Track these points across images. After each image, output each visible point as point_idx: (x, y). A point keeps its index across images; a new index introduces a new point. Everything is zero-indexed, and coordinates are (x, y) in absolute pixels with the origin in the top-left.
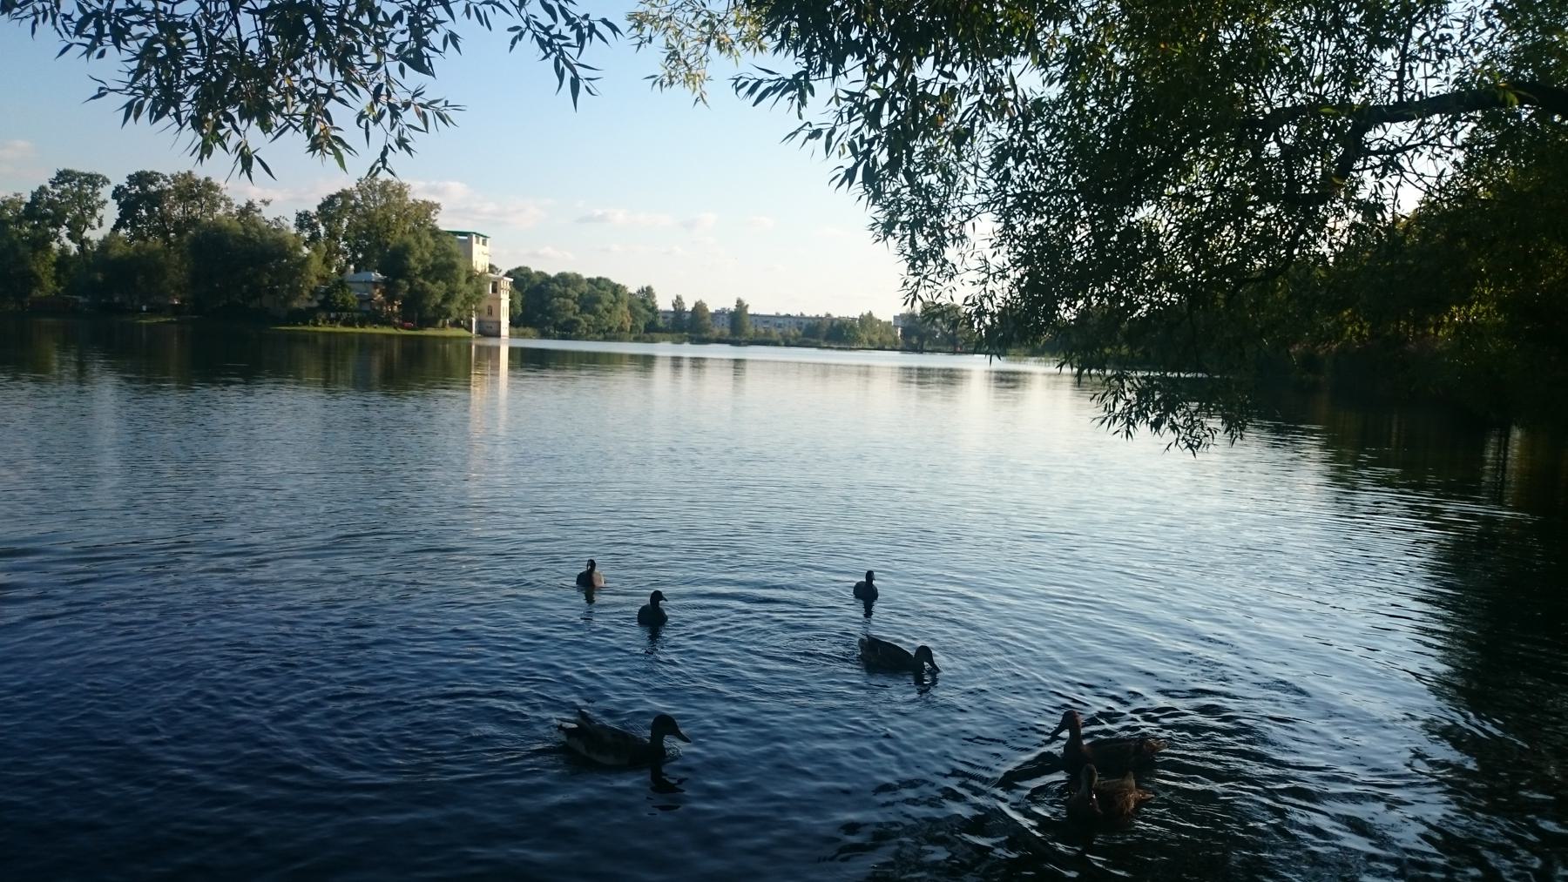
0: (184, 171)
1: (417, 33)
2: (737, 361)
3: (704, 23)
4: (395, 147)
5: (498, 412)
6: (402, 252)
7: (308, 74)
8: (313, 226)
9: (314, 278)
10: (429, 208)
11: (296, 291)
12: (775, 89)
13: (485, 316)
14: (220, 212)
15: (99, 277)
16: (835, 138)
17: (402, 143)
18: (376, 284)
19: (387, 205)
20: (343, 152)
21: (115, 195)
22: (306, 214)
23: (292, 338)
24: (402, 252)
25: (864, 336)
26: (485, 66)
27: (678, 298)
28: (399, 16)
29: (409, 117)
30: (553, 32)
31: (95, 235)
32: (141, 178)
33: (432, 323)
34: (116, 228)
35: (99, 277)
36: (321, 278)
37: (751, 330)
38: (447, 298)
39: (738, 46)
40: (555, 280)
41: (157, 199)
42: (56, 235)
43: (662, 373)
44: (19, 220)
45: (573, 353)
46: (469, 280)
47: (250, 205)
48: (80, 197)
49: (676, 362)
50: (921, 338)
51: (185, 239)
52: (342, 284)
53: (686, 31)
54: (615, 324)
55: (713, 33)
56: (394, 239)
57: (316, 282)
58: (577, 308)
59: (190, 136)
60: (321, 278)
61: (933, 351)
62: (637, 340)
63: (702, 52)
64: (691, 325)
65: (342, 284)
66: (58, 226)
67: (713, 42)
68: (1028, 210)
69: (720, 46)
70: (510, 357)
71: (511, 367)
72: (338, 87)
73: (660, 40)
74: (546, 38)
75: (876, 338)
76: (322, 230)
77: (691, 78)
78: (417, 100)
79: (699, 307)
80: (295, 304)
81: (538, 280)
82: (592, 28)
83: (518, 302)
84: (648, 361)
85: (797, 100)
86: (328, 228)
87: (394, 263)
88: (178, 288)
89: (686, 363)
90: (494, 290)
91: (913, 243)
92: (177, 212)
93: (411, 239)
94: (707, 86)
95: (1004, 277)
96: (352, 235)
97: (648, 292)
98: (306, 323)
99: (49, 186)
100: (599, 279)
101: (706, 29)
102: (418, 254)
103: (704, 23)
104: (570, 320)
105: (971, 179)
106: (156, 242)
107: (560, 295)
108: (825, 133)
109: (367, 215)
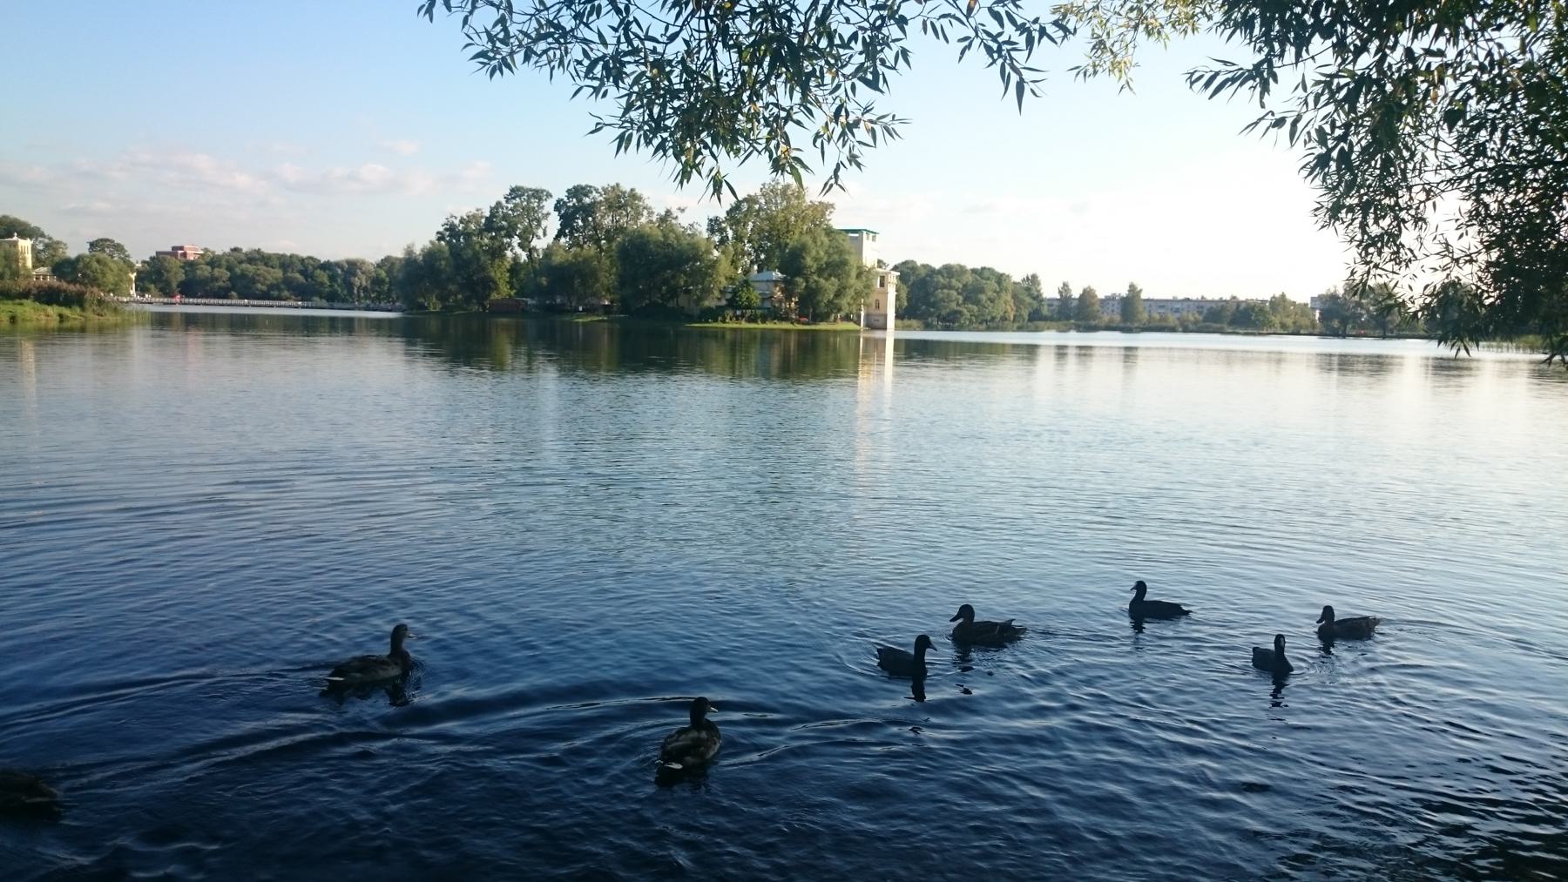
0: (613, 184)
1: (871, 50)
2: (1128, 349)
3: (1132, 9)
4: (846, 163)
5: (884, 403)
6: (798, 254)
7: (772, 99)
8: (722, 230)
9: (722, 279)
10: (409, 252)
11: (707, 291)
12: (1233, 80)
13: (873, 310)
14: (643, 220)
15: (544, 281)
16: (1300, 126)
17: (853, 159)
18: (776, 282)
19: (787, 208)
20: (801, 171)
21: (557, 208)
22: (716, 219)
23: (704, 335)
25: (1276, 320)
26: (935, 79)
27: (1065, 285)
28: (854, 37)
29: (861, 133)
30: (1000, 39)
31: (540, 244)
32: (577, 192)
33: (824, 317)
34: (557, 237)
35: (544, 281)
36: (731, 279)
38: (838, 295)
39: (1168, 29)
40: (939, 272)
41: (588, 210)
42: (510, 245)
43: (1046, 361)
44: (480, 233)
45: (956, 344)
46: (859, 276)
47: (668, 212)
48: (528, 210)
49: (1061, 351)
50: (1344, 322)
51: (614, 245)
52: (746, 283)
53: (1113, 20)
54: (998, 314)
55: (1142, 17)
56: (793, 241)
57: (724, 282)
58: (961, 299)
59: (672, 165)
60: (731, 279)
61: (1357, 336)
62: (1020, 329)
63: (1128, 38)
64: (1078, 313)
65: (746, 283)
66: (511, 237)
67: (1141, 27)
68: (1504, 183)
69: (1149, 34)
70: (896, 348)
71: (896, 359)
72: (796, 109)
73: (1085, 32)
74: (995, 46)
75: (1289, 321)
76: (730, 233)
77: (1115, 66)
78: (867, 116)
79: (1087, 294)
80: (706, 303)
81: (923, 272)
82: (1043, 32)
83: (904, 295)
84: (1031, 351)
85: (1258, 89)
86: (735, 232)
87: (792, 264)
88: (608, 290)
89: (1072, 352)
90: (882, 285)
91: (1363, 226)
92: (607, 221)
93: (807, 239)
94: (1132, 73)
95: (1471, 261)
96: (756, 237)
97: (1033, 280)
98: (716, 321)
99: (504, 201)
101: (1133, 15)
102: (814, 253)
103: (1132, 9)
104: (951, 310)
105: (1430, 154)
106: (590, 249)
107: (944, 287)
108: (1289, 122)
109: (770, 218)
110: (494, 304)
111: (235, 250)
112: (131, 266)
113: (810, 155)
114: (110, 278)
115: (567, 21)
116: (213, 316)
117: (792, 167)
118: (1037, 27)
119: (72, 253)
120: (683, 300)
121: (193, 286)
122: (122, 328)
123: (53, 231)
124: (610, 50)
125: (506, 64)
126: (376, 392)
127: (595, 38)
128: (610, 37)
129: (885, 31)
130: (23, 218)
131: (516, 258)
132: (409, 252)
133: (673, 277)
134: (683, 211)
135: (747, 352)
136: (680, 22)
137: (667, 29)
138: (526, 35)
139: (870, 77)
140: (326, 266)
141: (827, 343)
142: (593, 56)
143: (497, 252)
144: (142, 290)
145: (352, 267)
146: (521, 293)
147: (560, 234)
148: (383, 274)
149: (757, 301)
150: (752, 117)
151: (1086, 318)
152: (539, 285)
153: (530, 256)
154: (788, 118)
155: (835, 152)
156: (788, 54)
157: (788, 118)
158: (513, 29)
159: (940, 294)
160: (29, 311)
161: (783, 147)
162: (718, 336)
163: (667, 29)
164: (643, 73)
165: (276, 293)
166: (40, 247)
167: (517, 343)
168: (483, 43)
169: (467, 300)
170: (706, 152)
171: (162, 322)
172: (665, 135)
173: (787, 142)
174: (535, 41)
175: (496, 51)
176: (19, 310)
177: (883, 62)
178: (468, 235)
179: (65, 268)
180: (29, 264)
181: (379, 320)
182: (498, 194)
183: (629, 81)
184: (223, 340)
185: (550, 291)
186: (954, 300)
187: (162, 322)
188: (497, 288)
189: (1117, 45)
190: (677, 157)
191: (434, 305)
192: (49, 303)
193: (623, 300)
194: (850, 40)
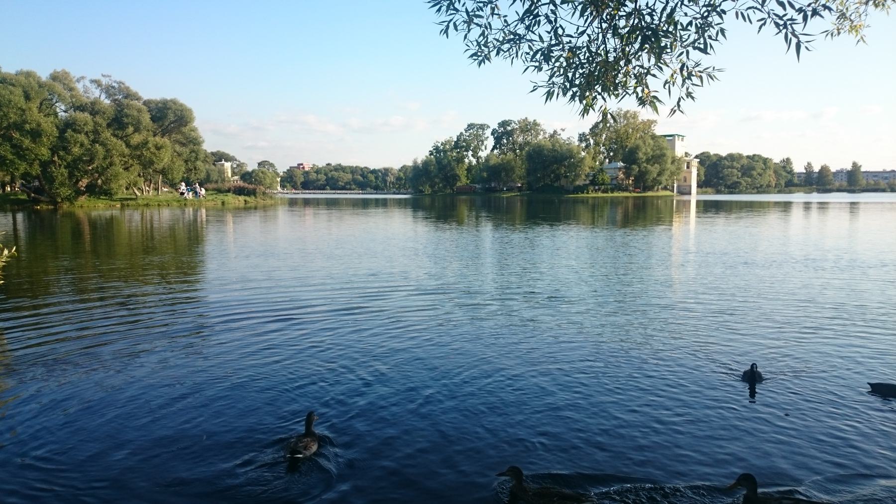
0: (524, 118)
2: (852, 203)
4: (685, 97)
5: (688, 242)
6: (634, 151)
7: (638, 63)
8: (587, 140)
9: (587, 169)
10: (415, 162)
11: (577, 176)
13: (682, 183)
14: (541, 137)
15: (485, 174)
17: (689, 95)
18: (620, 169)
19: (627, 124)
21: (492, 134)
22: (584, 134)
23: (576, 201)
24: (634, 151)
28: (690, 23)
29: (695, 80)
31: (483, 154)
32: (504, 124)
33: (651, 188)
34: (493, 150)
35: (485, 174)
37: (864, 182)
38: (659, 174)
40: (725, 158)
41: (509, 134)
43: (797, 213)
44: (452, 150)
45: (736, 202)
46: (673, 162)
47: (555, 132)
48: (477, 136)
49: (807, 206)
52: (602, 170)
54: (764, 182)
56: (630, 144)
58: (740, 174)
60: (592, 168)
62: (779, 192)
64: (818, 181)
65: (602, 170)
66: (467, 151)
69: (876, 6)
71: (697, 212)
74: (781, 22)
76: (592, 141)
77: (853, 28)
78: (697, 69)
80: (577, 183)
81: (715, 159)
83: (702, 173)
86: (595, 141)
87: (630, 158)
88: (520, 178)
89: (814, 206)
90: (688, 167)
92: (520, 139)
93: (640, 142)
94: (864, 32)
96: (607, 143)
97: (787, 161)
98: (583, 193)
100: (754, 155)
102: (644, 150)
104: (732, 181)
106: (510, 155)
107: (729, 167)
109: (616, 131)
110: (459, 188)
111: (328, 164)
112: (278, 174)
113: (662, 94)
114: (268, 181)
115: (521, 30)
116: (318, 199)
117: (651, 102)
118: (810, 8)
119: (250, 169)
120: (563, 182)
121: (307, 185)
122: (274, 206)
123: (241, 158)
124: (546, 45)
125: (487, 58)
126: (397, 240)
127: (537, 38)
128: (546, 37)
129: (710, 19)
130: (227, 151)
131: (470, 162)
132: (415, 162)
133: (558, 169)
134: (563, 130)
135: (602, 211)
136: (586, 25)
137: (578, 29)
138: (498, 40)
139: (702, 46)
140: (374, 172)
141: (653, 204)
142: (535, 49)
143: (460, 160)
144: (283, 187)
145: (386, 172)
146: (472, 182)
147: (494, 148)
148: (402, 175)
149: (608, 180)
150: (626, 74)
151: (824, 184)
152: (482, 177)
153: (478, 162)
154: (648, 73)
155: (677, 91)
156: (653, 37)
157: (648, 73)
158: (490, 38)
159: (726, 172)
160: (231, 198)
161: (646, 91)
162: (584, 202)
163: (578, 29)
164: (561, 55)
165: (348, 187)
166: (235, 166)
167: (470, 210)
168: (474, 49)
169: (445, 187)
170: (599, 97)
171: (292, 203)
172: (575, 89)
173: (647, 87)
174: (502, 43)
175: (482, 52)
176: (226, 198)
177: (710, 37)
178: (445, 152)
179: (247, 177)
180: (230, 175)
181: (400, 199)
182: (461, 128)
183: (553, 60)
184: (323, 212)
185: (488, 180)
186: (735, 175)
187: (292, 203)
188: (460, 180)
189: (853, 16)
190: (581, 102)
191: (428, 190)
192: (240, 195)
193: (529, 183)
194: (687, 26)
